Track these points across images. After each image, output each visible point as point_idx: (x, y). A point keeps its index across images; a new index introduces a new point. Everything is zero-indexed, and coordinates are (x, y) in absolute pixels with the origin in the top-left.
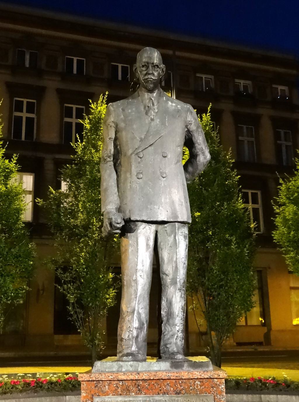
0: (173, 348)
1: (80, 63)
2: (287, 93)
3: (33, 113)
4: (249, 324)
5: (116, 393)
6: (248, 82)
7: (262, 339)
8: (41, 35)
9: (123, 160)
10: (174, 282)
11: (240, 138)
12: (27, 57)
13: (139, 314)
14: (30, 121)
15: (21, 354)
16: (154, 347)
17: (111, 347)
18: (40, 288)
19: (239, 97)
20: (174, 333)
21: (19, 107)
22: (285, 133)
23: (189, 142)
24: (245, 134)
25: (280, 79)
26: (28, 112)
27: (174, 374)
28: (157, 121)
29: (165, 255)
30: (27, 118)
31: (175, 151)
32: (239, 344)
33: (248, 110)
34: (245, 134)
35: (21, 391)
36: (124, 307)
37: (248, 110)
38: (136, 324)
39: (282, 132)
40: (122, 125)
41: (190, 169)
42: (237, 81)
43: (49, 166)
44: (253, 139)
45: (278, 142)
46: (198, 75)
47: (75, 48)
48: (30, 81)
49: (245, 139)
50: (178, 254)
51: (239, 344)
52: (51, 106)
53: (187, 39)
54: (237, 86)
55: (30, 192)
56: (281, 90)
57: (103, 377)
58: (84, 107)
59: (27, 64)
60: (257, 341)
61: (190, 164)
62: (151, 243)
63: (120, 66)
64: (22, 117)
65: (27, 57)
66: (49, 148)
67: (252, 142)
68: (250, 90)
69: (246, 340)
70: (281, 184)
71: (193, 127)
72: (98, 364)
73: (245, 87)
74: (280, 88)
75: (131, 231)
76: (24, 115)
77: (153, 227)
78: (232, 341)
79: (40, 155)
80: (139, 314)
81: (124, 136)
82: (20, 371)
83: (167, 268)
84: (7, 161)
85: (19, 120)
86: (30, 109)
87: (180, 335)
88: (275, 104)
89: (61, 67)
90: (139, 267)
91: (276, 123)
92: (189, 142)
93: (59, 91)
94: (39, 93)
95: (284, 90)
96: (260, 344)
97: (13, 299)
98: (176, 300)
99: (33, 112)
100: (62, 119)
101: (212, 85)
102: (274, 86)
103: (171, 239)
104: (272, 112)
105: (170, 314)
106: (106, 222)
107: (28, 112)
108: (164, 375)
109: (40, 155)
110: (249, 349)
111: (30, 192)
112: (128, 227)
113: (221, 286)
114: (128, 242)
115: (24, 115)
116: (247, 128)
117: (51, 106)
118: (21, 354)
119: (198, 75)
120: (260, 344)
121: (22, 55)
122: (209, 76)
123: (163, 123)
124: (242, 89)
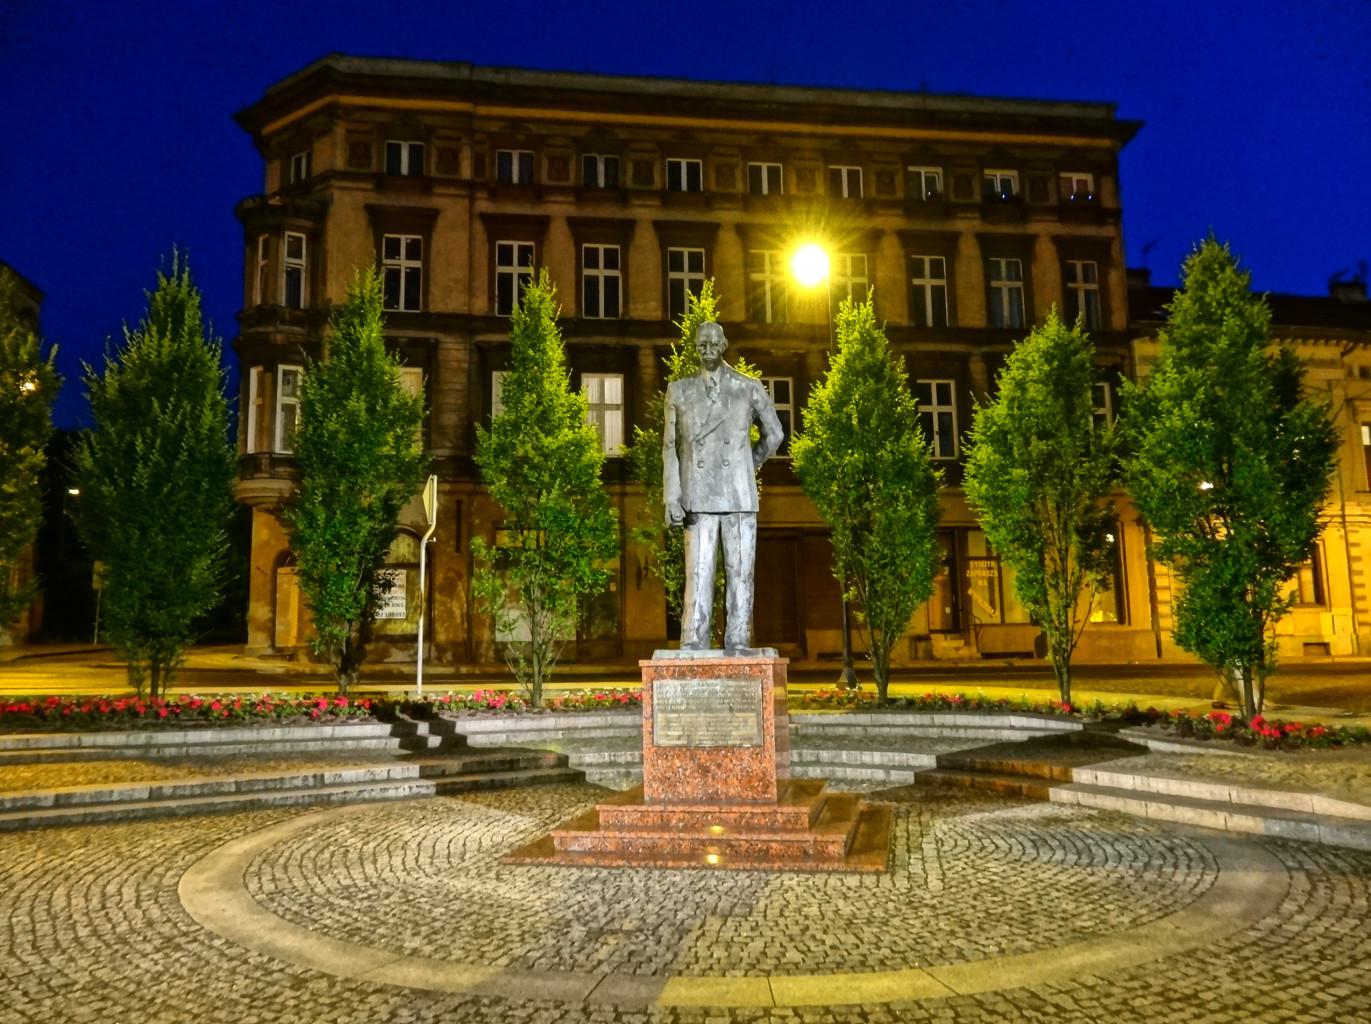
0: (735, 639)
1: (693, 169)
2: (1091, 187)
3: (616, 268)
4: (1008, 620)
5: (673, 677)
6: (1012, 174)
7: (1031, 648)
8: (622, 126)
9: (685, 446)
10: (739, 574)
11: (994, 284)
12: (601, 168)
13: (701, 607)
14: (611, 283)
15: (616, 668)
16: (718, 634)
17: (673, 634)
18: (643, 564)
19: (992, 205)
20: (740, 625)
21: (592, 260)
22: (1085, 267)
23: (757, 421)
24: (1004, 275)
25: (1075, 160)
26: (606, 267)
27: (726, 661)
28: (719, 404)
29: (730, 546)
30: (607, 278)
31: (740, 432)
32: (987, 656)
33: (1005, 229)
34: (1004, 275)
35: (608, 709)
36: (688, 599)
37: (1005, 229)
38: (697, 616)
39: (1079, 265)
40: (683, 408)
41: (760, 450)
42: (987, 172)
43: (647, 360)
44: (1019, 284)
45: (1070, 285)
46: (911, 169)
47: (684, 141)
48: (608, 212)
49: (1004, 285)
50: (743, 547)
51: (987, 656)
52: (645, 252)
53: (888, 102)
54: (988, 184)
55: (617, 407)
56: (1078, 181)
57: (661, 663)
58: (703, 250)
59: (601, 182)
60: (1022, 649)
61: (757, 446)
62: (715, 535)
63: (764, 166)
64: (597, 278)
65: (601, 168)
66: (646, 328)
67: (1018, 289)
68: (1015, 189)
69: (1000, 649)
70: (976, 412)
71: (760, 406)
72: (658, 653)
73: (1006, 183)
74: (1075, 177)
75: (692, 522)
76: (602, 273)
77: (717, 518)
78: (974, 650)
79: (633, 341)
80: (701, 607)
81: (687, 420)
82: (608, 686)
83: (732, 559)
84: (573, 395)
85: (592, 282)
86: (611, 263)
87: (744, 626)
88: (1065, 211)
89: (659, 180)
90: (702, 560)
91: (1065, 248)
92: (757, 421)
93: (657, 225)
94: (624, 231)
95: (1085, 182)
96: (1028, 655)
97: (591, 587)
98: (742, 594)
99: (615, 267)
100: (665, 276)
101: (940, 186)
102: (1064, 175)
103: (735, 529)
104: (1058, 229)
105: (734, 606)
106: (667, 515)
107: (606, 267)
108: (716, 662)
109: (633, 341)
110: (1018, 663)
111: (617, 407)
112: (690, 519)
113: (884, 566)
114: (691, 535)
115: (602, 273)
116: (1008, 263)
117: (645, 252)
118: (616, 668)
119: (911, 169)
120: (1028, 655)
121: (591, 165)
122: (932, 169)
123: (725, 405)
124: (998, 188)
